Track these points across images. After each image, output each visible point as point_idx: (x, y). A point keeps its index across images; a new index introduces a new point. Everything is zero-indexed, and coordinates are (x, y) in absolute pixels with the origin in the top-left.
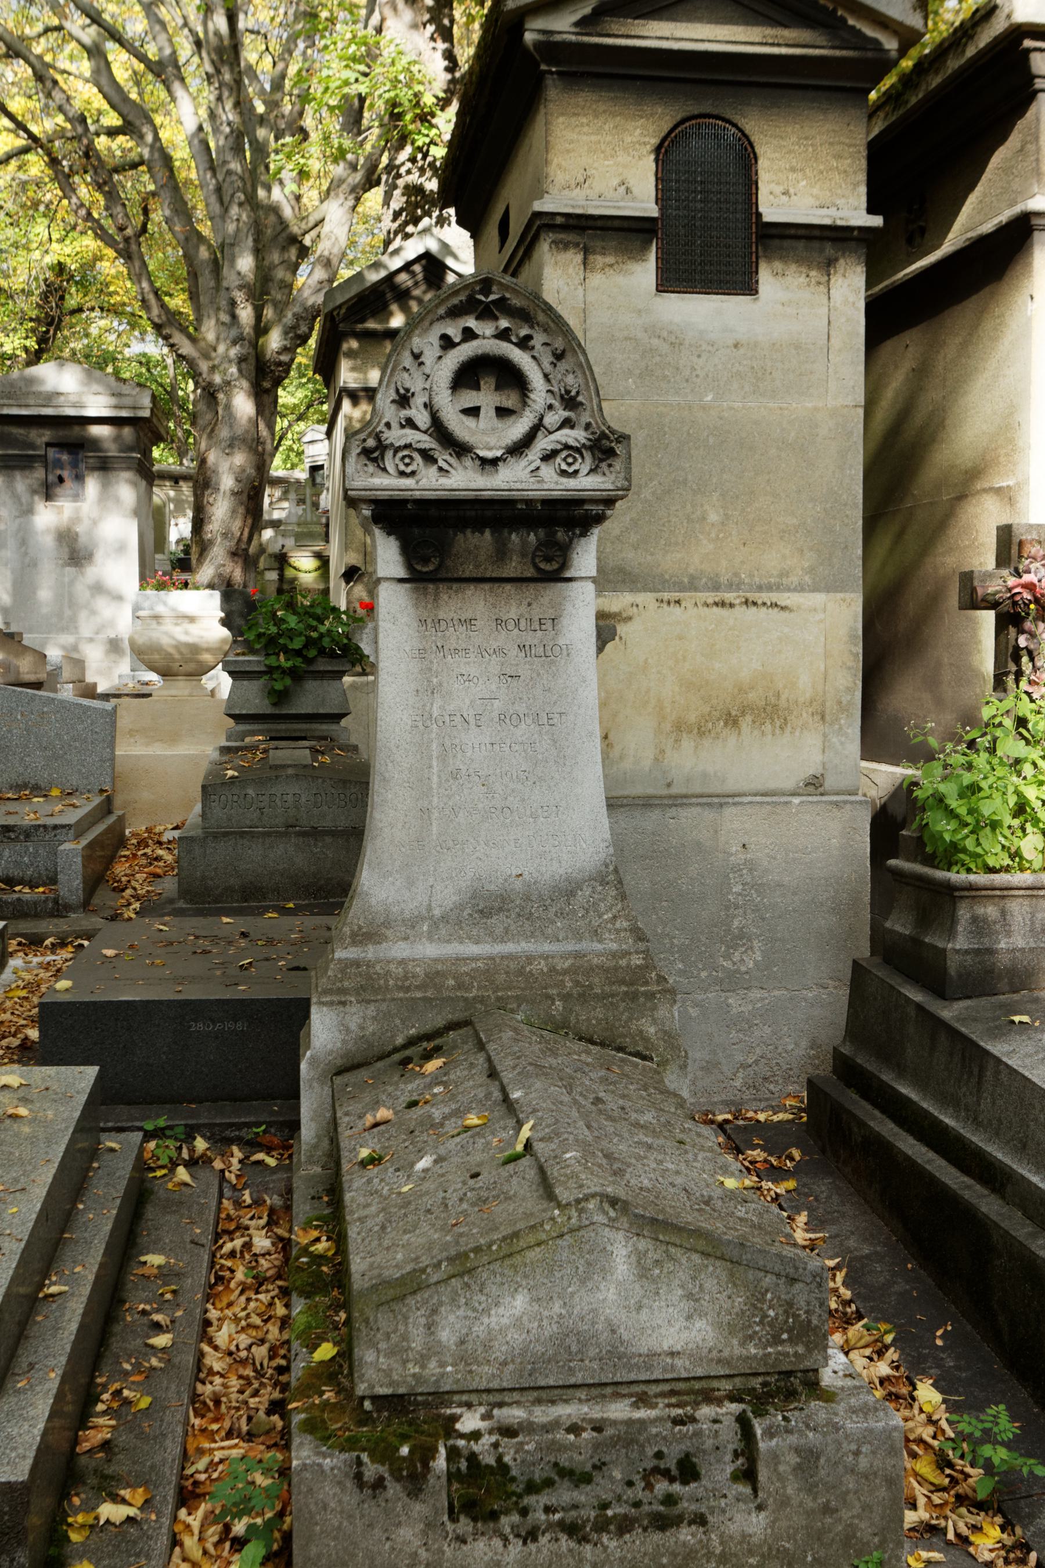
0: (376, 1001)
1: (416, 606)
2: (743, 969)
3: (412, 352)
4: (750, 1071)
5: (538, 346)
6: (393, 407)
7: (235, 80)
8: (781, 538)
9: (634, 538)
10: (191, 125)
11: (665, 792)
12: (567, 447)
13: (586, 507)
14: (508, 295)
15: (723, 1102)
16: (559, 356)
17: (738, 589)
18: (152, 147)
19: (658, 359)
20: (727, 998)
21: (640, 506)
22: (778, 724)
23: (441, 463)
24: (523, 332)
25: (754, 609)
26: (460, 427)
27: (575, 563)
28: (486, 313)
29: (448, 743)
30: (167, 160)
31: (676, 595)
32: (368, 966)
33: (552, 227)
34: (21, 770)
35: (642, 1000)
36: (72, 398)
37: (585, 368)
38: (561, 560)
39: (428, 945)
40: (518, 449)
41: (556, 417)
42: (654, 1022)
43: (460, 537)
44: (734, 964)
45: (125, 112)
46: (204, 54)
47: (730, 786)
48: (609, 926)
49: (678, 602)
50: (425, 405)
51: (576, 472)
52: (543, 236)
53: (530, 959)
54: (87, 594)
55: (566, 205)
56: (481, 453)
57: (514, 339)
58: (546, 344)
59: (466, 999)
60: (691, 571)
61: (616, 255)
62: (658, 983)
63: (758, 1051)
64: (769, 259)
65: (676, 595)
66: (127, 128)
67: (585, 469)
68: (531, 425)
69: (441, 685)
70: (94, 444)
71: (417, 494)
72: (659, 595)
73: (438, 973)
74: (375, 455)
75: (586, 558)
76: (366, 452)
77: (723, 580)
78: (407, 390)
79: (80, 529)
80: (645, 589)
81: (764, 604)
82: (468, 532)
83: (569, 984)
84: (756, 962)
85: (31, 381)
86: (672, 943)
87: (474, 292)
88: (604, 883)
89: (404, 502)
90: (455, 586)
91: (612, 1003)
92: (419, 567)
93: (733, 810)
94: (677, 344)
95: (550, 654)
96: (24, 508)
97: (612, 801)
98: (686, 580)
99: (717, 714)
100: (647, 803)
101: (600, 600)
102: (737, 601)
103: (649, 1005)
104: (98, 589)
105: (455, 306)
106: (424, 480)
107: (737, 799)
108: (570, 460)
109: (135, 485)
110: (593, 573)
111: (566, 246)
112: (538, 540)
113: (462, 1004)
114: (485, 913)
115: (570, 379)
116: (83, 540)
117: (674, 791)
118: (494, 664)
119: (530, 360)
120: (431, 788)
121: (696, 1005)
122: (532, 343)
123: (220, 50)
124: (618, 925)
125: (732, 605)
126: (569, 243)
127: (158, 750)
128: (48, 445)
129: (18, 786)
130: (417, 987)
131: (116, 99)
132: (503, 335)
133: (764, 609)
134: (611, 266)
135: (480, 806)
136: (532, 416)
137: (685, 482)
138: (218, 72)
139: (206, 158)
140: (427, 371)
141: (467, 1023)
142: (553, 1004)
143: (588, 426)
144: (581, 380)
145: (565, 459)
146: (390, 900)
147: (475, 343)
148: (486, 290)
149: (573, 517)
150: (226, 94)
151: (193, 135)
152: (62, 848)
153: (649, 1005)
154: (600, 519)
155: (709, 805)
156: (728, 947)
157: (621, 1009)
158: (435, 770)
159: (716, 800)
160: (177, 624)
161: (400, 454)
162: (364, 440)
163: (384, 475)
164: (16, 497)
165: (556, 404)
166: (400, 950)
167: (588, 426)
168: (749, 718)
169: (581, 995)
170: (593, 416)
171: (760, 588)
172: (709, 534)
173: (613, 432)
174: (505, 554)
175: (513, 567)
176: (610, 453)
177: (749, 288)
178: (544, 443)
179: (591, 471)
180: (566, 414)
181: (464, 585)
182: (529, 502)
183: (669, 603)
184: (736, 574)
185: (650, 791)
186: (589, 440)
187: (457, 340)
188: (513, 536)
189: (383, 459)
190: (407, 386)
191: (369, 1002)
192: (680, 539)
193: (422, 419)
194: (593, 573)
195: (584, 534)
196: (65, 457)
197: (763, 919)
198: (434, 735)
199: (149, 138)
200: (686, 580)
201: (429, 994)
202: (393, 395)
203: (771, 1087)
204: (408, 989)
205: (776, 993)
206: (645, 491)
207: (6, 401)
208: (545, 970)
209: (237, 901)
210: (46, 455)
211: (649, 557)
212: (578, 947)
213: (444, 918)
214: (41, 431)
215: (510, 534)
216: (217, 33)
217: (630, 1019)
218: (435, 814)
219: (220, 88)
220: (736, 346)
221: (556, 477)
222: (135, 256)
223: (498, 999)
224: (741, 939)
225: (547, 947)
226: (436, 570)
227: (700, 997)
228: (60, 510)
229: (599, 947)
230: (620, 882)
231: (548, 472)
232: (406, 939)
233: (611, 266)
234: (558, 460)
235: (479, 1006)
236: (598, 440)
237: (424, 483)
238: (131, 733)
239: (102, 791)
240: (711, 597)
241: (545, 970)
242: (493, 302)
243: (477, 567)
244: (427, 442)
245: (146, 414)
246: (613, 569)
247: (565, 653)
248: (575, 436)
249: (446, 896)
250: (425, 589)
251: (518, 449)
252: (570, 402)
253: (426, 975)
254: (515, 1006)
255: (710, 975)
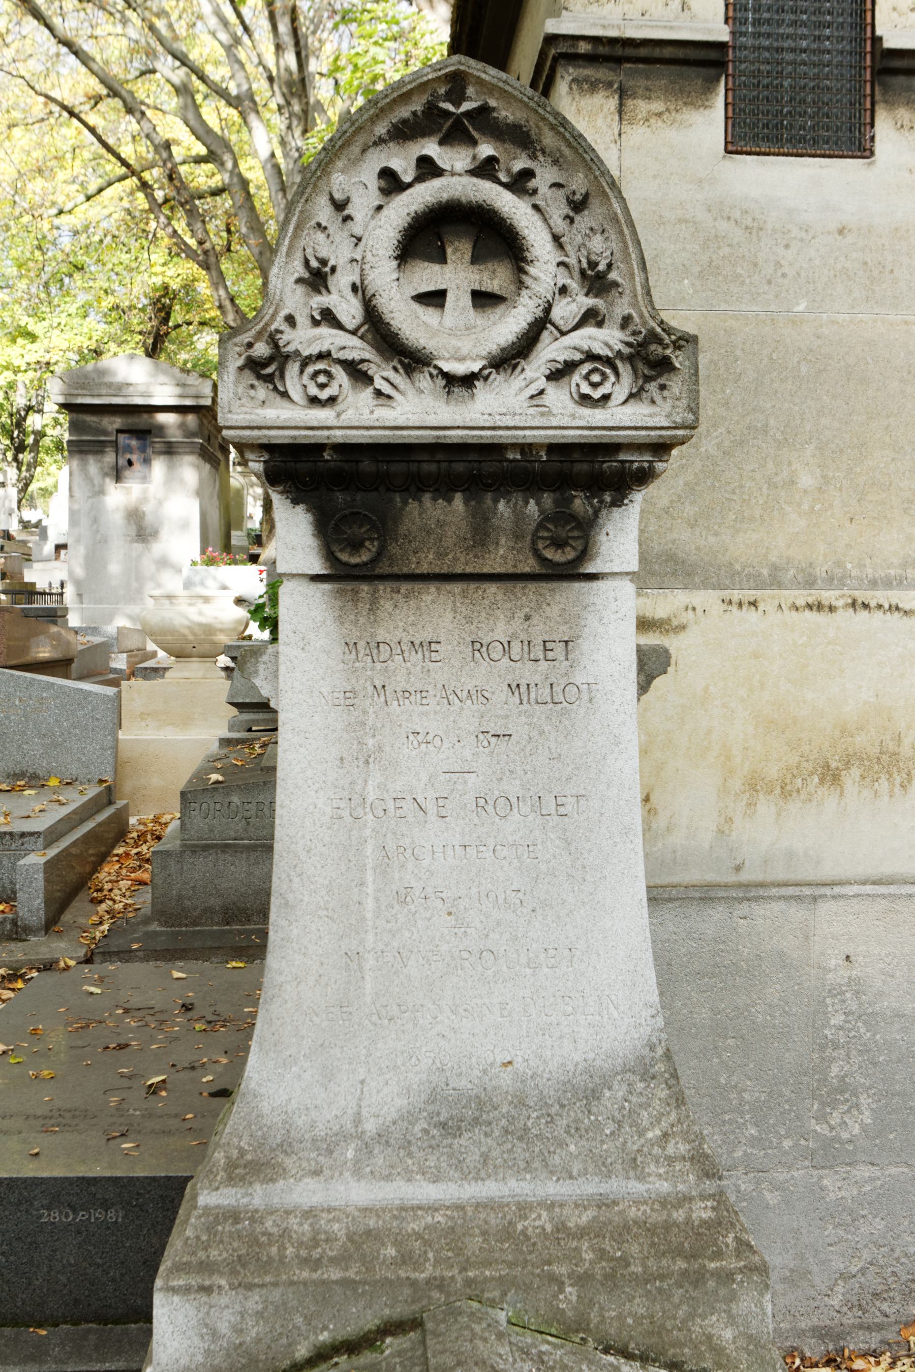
0: (262, 1286)
1: (340, 620)
2: (845, 1136)
3: (332, 199)
4: (854, 1283)
5: (543, 189)
6: (300, 290)
7: (303, 110)
8: (905, 511)
9: (689, 510)
10: (264, 153)
11: (732, 878)
12: (591, 357)
13: (623, 457)
14: (493, 103)
15: (814, 1329)
16: (578, 205)
17: (842, 584)
18: (232, 172)
19: (726, 250)
20: (821, 1178)
21: (698, 464)
22: (898, 780)
23: (379, 383)
24: (519, 165)
25: (865, 613)
26: (412, 324)
27: (604, 549)
28: (456, 133)
29: (391, 846)
30: (244, 183)
31: (751, 594)
32: (252, 1220)
33: (573, 58)
34: (19, 758)
35: (711, 1284)
36: (141, 389)
37: (623, 225)
38: (579, 545)
39: (353, 1184)
40: (509, 359)
41: (574, 307)
42: (732, 1320)
43: (413, 506)
44: (832, 1128)
45: (209, 142)
46: (276, 88)
47: (828, 871)
48: (656, 1150)
49: (754, 604)
50: (354, 288)
51: (606, 398)
52: (560, 71)
53: (524, 1208)
54: (153, 568)
55: (594, 25)
56: (446, 367)
57: (504, 178)
58: (557, 185)
59: (414, 1283)
60: (773, 558)
61: (667, 100)
62: (738, 1255)
63: (866, 1255)
64: (891, 104)
65: (751, 594)
66: (211, 157)
67: (621, 392)
68: (530, 319)
69: (380, 749)
70: (160, 429)
71: (338, 436)
72: (726, 594)
73: (368, 1232)
74: (269, 370)
75: (621, 538)
76: (254, 366)
77: (820, 571)
78: (323, 262)
79: (147, 508)
80: (706, 585)
81: (880, 606)
82: (427, 497)
83: (588, 1256)
84: (864, 1127)
85: (102, 373)
86: (742, 1099)
87: (435, 96)
88: (647, 1076)
89: (319, 448)
90: (405, 587)
91: (660, 1290)
92: (344, 557)
93: (832, 906)
94: (754, 231)
95: (559, 699)
96: (97, 489)
97: (655, 892)
98: (765, 572)
99: (810, 766)
100: (706, 895)
101: (642, 600)
102: (840, 603)
103: (722, 1292)
104: (164, 563)
105: (404, 122)
106: (350, 412)
107: (837, 890)
108: (596, 378)
109: (198, 467)
110: (634, 566)
111: (593, 86)
112: (542, 512)
113: (407, 1291)
114: (450, 1128)
115: (597, 244)
116: (149, 519)
117: (746, 876)
118: (468, 716)
119: (530, 211)
120: (364, 919)
121: (775, 1187)
122: (532, 184)
123: (290, 84)
124: (670, 1150)
125: (832, 609)
126: (598, 81)
127: (169, 734)
128: (119, 431)
129: (15, 774)
130: (333, 1261)
131: (201, 131)
132: (485, 169)
133: (879, 614)
134: (659, 115)
135: (444, 948)
136: (531, 304)
137: (765, 430)
138: (288, 103)
139: (277, 181)
140: (358, 231)
141: (414, 1324)
142: (561, 1290)
143: (626, 321)
144: (615, 245)
145: (587, 377)
146: (294, 1105)
147: (436, 183)
148: (457, 96)
149: (596, 474)
150: (295, 123)
151: (266, 161)
152: (22, 862)
153: (722, 1292)
154: (644, 477)
155: (798, 898)
156: (823, 1104)
157: (676, 1300)
158: (370, 889)
159: (807, 891)
160: (190, 605)
161: (310, 369)
162: (250, 345)
163: (285, 403)
164: (89, 479)
165: (574, 285)
166: (302, 1192)
167: (626, 321)
168: (855, 772)
169: (610, 1277)
170: (634, 304)
171: (873, 584)
172: (799, 505)
173: (668, 331)
174: (487, 534)
175: (499, 559)
176: (664, 366)
177: (862, 149)
178: (551, 351)
179: (631, 396)
180: (590, 302)
181: (418, 586)
182: (526, 448)
183: (740, 605)
184: (839, 564)
185: (711, 877)
186: (628, 344)
187: (407, 178)
188: (501, 505)
189: (282, 377)
190: (323, 254)
191: (250, 1287)
192: (758, 512)
193: (349, 310)
194: (634, 566)
195: (617, 502)
196: (134, 443)
197: (875, 1064)
198: (368, 832)
199: (229, 165)
200: (765, 572)
201: (351, 1274)
202: (300, 271)
203: (885, 1307)
204: (317, 1264)
205: (893, 1170)
206: (707, 441)
207: (80, 392)
208: (549, 1228)
209: (218, 924)
210: (116, 441)
211: (712, 539)
212: (604, 1188)
213: (382, 1137)
214: (113, 419)
215: (496, 501)
216: (287, 69)
217: (691, 1316)
218: (370, 962)
219: (290, 118)
220: (841, 232)
221: (571, 407)
222: (213, 267)
223: (469, 1282)
224: (840, 1093)
225: (552, 1189)
226: (374, 561)
227: (781, 1176)
228: (128, 491)
229: (636, 1187)
230: (675, 1076)
231: (559, 399)
232: (317, 1173)
233: (659, 115)
234: (576, 378)
235: (435, 1294)
236: (643, 345)
237: (350, 416)
238: (143, 716)
239: (101, 781)
240: (802, 597)
241: (549, 1228)
242: (468, 114)
243: (441, 555)
244: (356, 348)
245: (208, 402)
246: (659, 556)
247: (585, 696)
248: (606, 339)
249: (387, 1101)
250: (356, 592)
251: (509, 359)
252: (596, 281)
253: (350, 1237)
254: (496, 1294)
255: (796, 1145)
